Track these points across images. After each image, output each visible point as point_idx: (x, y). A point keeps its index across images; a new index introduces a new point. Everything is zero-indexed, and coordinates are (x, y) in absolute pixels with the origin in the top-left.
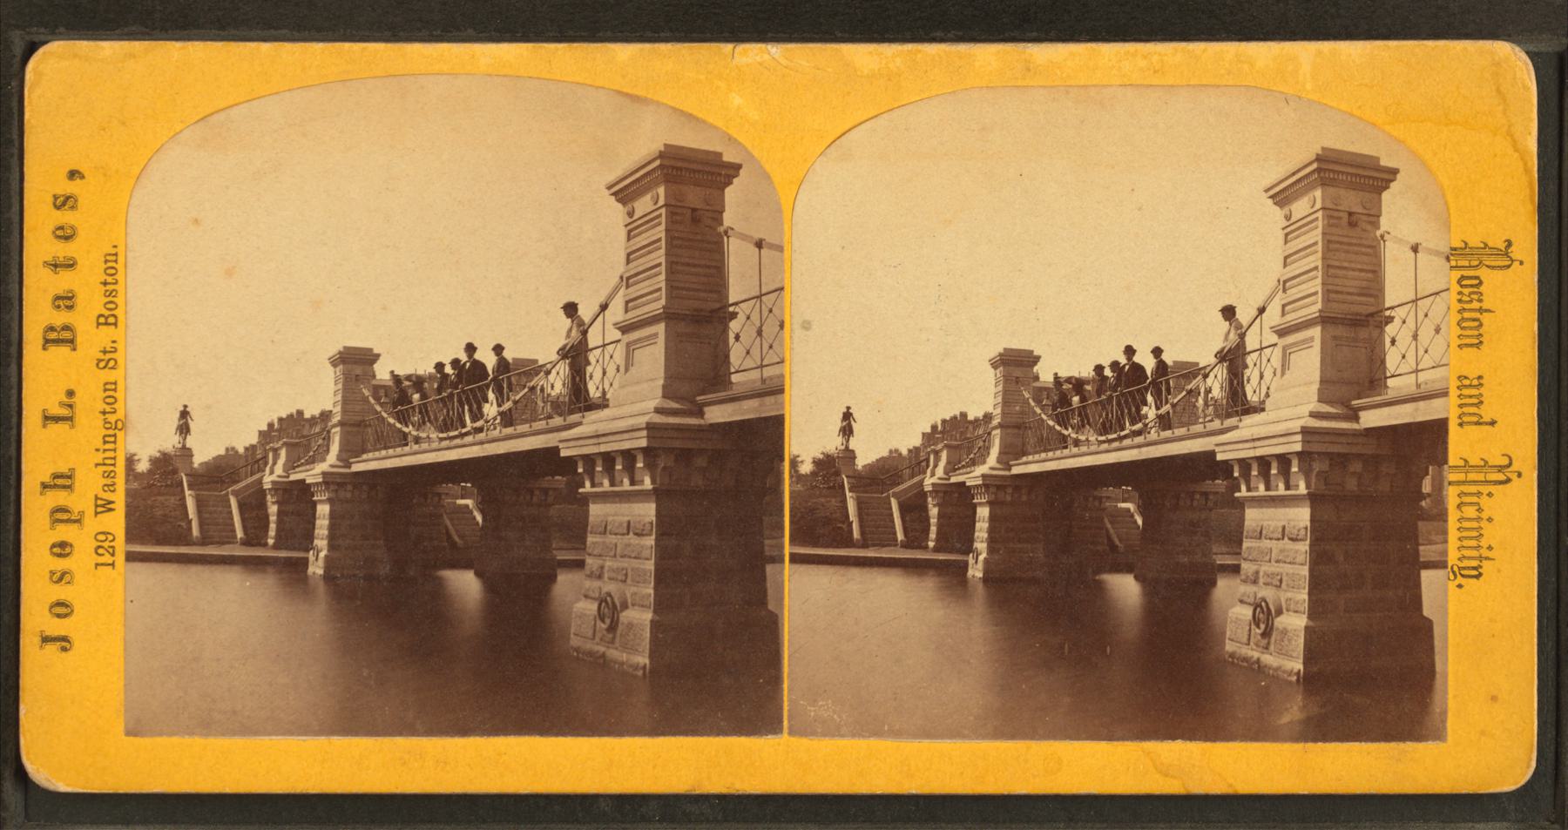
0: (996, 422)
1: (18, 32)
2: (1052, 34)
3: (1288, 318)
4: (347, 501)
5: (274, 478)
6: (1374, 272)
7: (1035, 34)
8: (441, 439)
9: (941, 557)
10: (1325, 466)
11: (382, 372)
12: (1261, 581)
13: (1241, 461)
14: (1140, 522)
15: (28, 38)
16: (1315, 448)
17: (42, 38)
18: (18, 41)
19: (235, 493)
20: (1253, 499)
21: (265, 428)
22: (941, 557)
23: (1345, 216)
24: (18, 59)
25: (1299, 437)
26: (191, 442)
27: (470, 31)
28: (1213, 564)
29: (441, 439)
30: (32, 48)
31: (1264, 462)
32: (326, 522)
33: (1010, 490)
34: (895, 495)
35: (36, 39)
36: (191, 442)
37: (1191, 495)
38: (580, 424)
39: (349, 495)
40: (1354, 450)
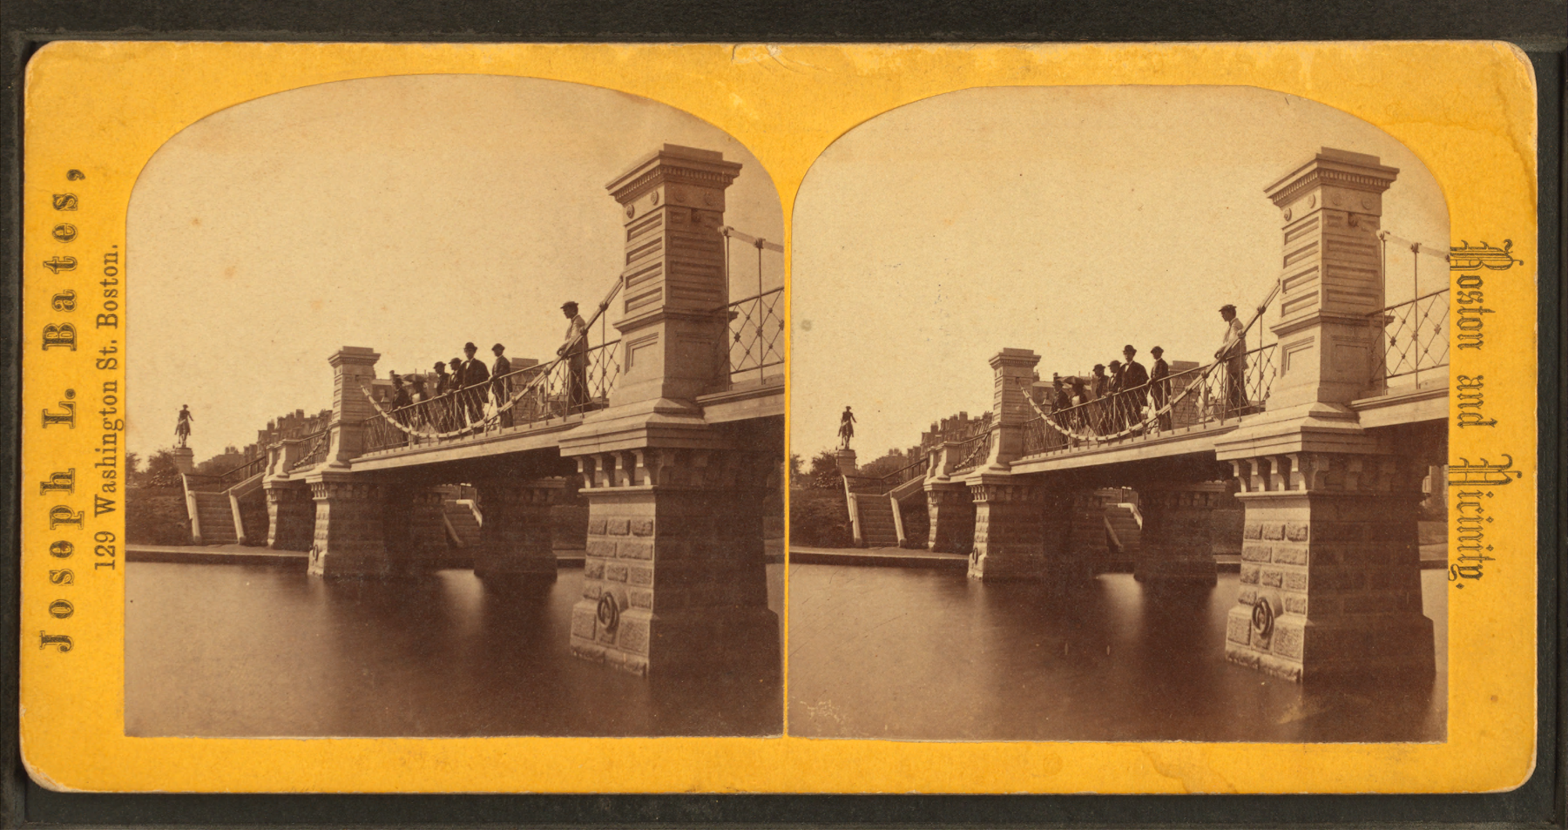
0: (995, 422)
1: (18, 32)
2: (1053, 34)
3: (1288, 318)
4: (347, 501)
5: (274, 478)
6: (1374, 272)
7: (1035, 34)
8: (442, 439)
9: (941, 557)
10: (1325, 466)
11: (382, 372)
12: (1261, 581)
13: (1241, 461)
14: (1140, 522)
15: (27, 38)
16: (1315, 448)
17: (42, 38)
18: (18, 41)
19: (235, 493)
20: (1253, 499)
21: (265, 428)
22: (941, 557)
23: (1345, 216)
24: (18, 59)
25: (1299, 437)
26: (191, 442)
27: (470, 31)
28: (1213, 564)
29: (442, 439)
30: (32, 48)
31: (1264, 462)
32: (326, 522)
33: (1009, 490)
34: (895, 495)
35: (36, 39)
36: (191, 442)
37: (1191, 495)
38: (580, 424)
39: (349, 495)
40: (1354, 450)
